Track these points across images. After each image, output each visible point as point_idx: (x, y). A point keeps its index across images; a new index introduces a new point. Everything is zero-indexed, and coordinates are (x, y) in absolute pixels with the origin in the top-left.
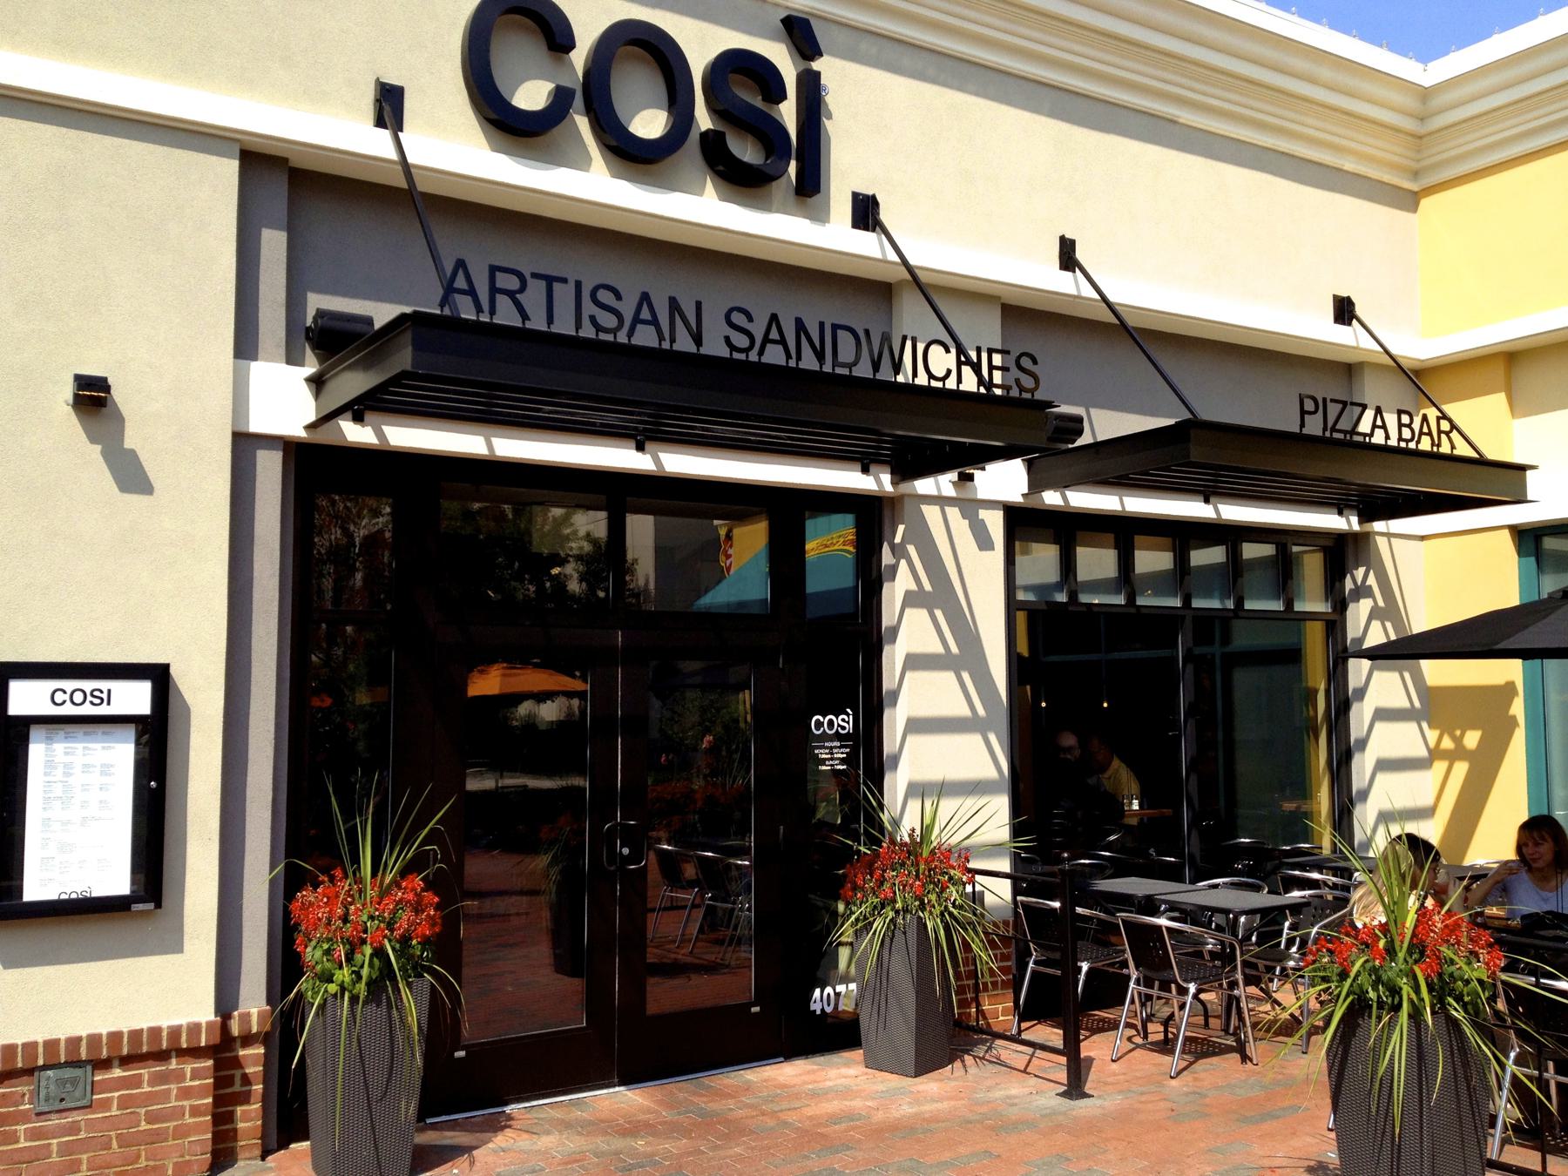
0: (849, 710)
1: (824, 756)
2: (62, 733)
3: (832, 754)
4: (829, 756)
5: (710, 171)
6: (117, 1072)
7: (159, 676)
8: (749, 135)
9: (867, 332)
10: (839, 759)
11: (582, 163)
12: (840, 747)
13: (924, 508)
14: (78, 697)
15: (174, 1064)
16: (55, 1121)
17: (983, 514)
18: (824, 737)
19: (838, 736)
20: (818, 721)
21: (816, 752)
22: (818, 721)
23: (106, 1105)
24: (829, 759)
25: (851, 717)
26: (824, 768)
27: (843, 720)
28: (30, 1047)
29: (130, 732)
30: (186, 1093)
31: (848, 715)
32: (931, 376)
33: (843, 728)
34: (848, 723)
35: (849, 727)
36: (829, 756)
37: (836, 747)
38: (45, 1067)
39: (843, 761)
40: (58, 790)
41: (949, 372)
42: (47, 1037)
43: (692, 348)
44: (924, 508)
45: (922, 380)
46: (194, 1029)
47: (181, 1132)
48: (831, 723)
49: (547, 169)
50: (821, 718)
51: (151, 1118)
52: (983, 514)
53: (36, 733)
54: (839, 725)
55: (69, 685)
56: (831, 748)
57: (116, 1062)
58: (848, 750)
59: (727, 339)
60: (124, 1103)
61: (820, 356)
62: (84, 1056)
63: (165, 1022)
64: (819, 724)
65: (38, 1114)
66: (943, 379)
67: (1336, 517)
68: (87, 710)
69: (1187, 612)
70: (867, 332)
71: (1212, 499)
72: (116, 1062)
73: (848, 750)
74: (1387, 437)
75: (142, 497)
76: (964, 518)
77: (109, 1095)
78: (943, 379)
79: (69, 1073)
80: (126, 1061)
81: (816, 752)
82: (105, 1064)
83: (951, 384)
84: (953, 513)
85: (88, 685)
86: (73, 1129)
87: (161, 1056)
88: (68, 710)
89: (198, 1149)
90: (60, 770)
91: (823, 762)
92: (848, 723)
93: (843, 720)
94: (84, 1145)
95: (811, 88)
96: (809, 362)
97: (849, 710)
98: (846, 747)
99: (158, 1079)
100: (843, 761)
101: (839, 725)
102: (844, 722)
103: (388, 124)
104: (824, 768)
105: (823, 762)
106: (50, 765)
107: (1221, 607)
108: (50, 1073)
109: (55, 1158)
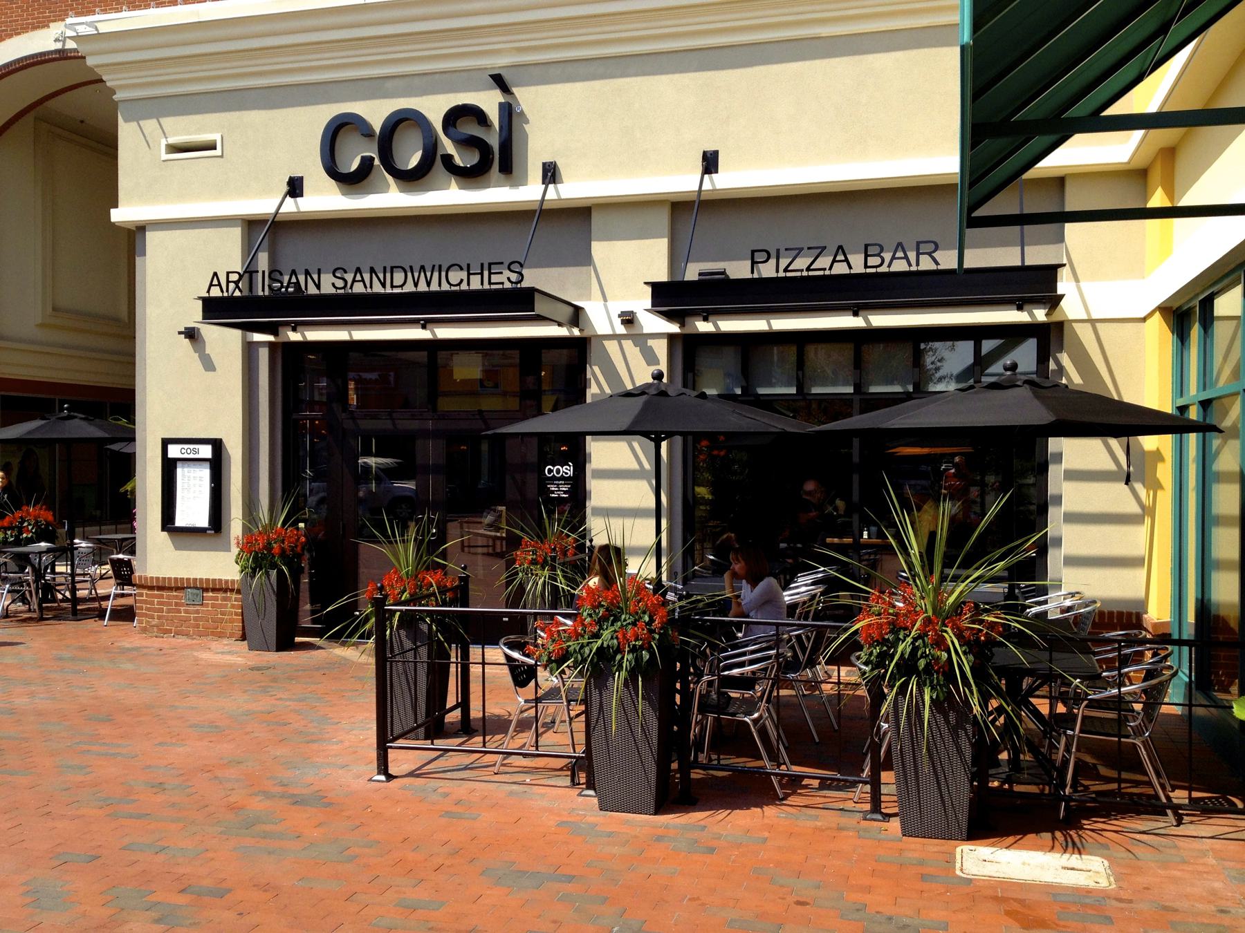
0: (570, 463)
1: (553, 489)
2: (186, 465)
3: (559, 488)
4: (557, 489)
5: (452, 175)
6: (211, 594)
7: (217, 445)
8: (477, 150)
9: (411, 268)
10: (563, 491)
11: (384, 189)
12: (564, 484)
13: (606, 343)
14: (189, 451)
15: (229, 594)
16: (192, 608)
17: (650, 342)
18: (554, 478)
19: (562, 478)
20: (549, 469)
21: (549, 486)
22: (549, 469)
23: (207, 605)
24: (556, 491)
25: (572, 467)
26: (553, 495)
27: (566, 469)
28: (188, 580)
29: (208, 465)
30: (233, 606)
31: (570, 466)
32: (451, 285)
33: (567, 473)
34: (570, 470)
35: (571, 473)
36: (557, 489)
37: (561, 484)
38: (187, 588)
39: (565, 492)
40: (186, 486)
41: (462, 280)
42: (187, 577)
43: (317, 292)
44: (606, 343)
45: (445, 287)
46: (233, 581)
47: (232, 621)
48: (558, 471)
49: (362, 198)
50: (552, 468)
51: (147, 609)
52: (650, 342)
53: (179, 464)
54: (563, 472)
55: (186, 446)
56: (558, 485)
57: (210, 590)
58: (569, 486)
59: (333, 284)
60: (159, 603)
61: (384, 285)
62: (173, 585)
63: (224, 578)
64: (550, 471)
65: (187, 604)
66: (459, 284)
67: (1016, 312)
68: (191, 456)
69: (857, 398)
70: (411, 268)
71: (860, 313)
72: (210, 590)
73: (569, 486)
74: (910, 265)
75: (212, 373)
76: (636, 346)
77: (813, 623)
78: (459, 284)
79: (195, 591)
80: (214, 590)
81: (549, 486)
82: (206, 590)
83: (464, 287)
84: (628, 345)
85: (192, 446)
86: (197, 612)
87: (226, 591)
88: (186, 456)
89: (237, 629)
90: (187, 479)
91: (553, 492)
92: (570, 470)
93: (566, 469)
94: (201, 619)
95: (508, 111)
96: (377, 288)
97: (570, 463)
98: (568, 484)
99: (224, 599)
100: (565, 492)
101: (563, 472)
102: (568, 470)
103: (976, 35)
104: (553, 495)
105: (553, 492)
106: (183, 475)
107: (902, 391)
108: (189, 590)
109: (192, 622)
